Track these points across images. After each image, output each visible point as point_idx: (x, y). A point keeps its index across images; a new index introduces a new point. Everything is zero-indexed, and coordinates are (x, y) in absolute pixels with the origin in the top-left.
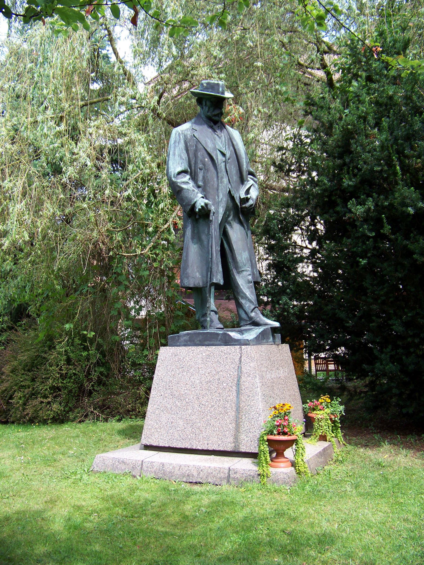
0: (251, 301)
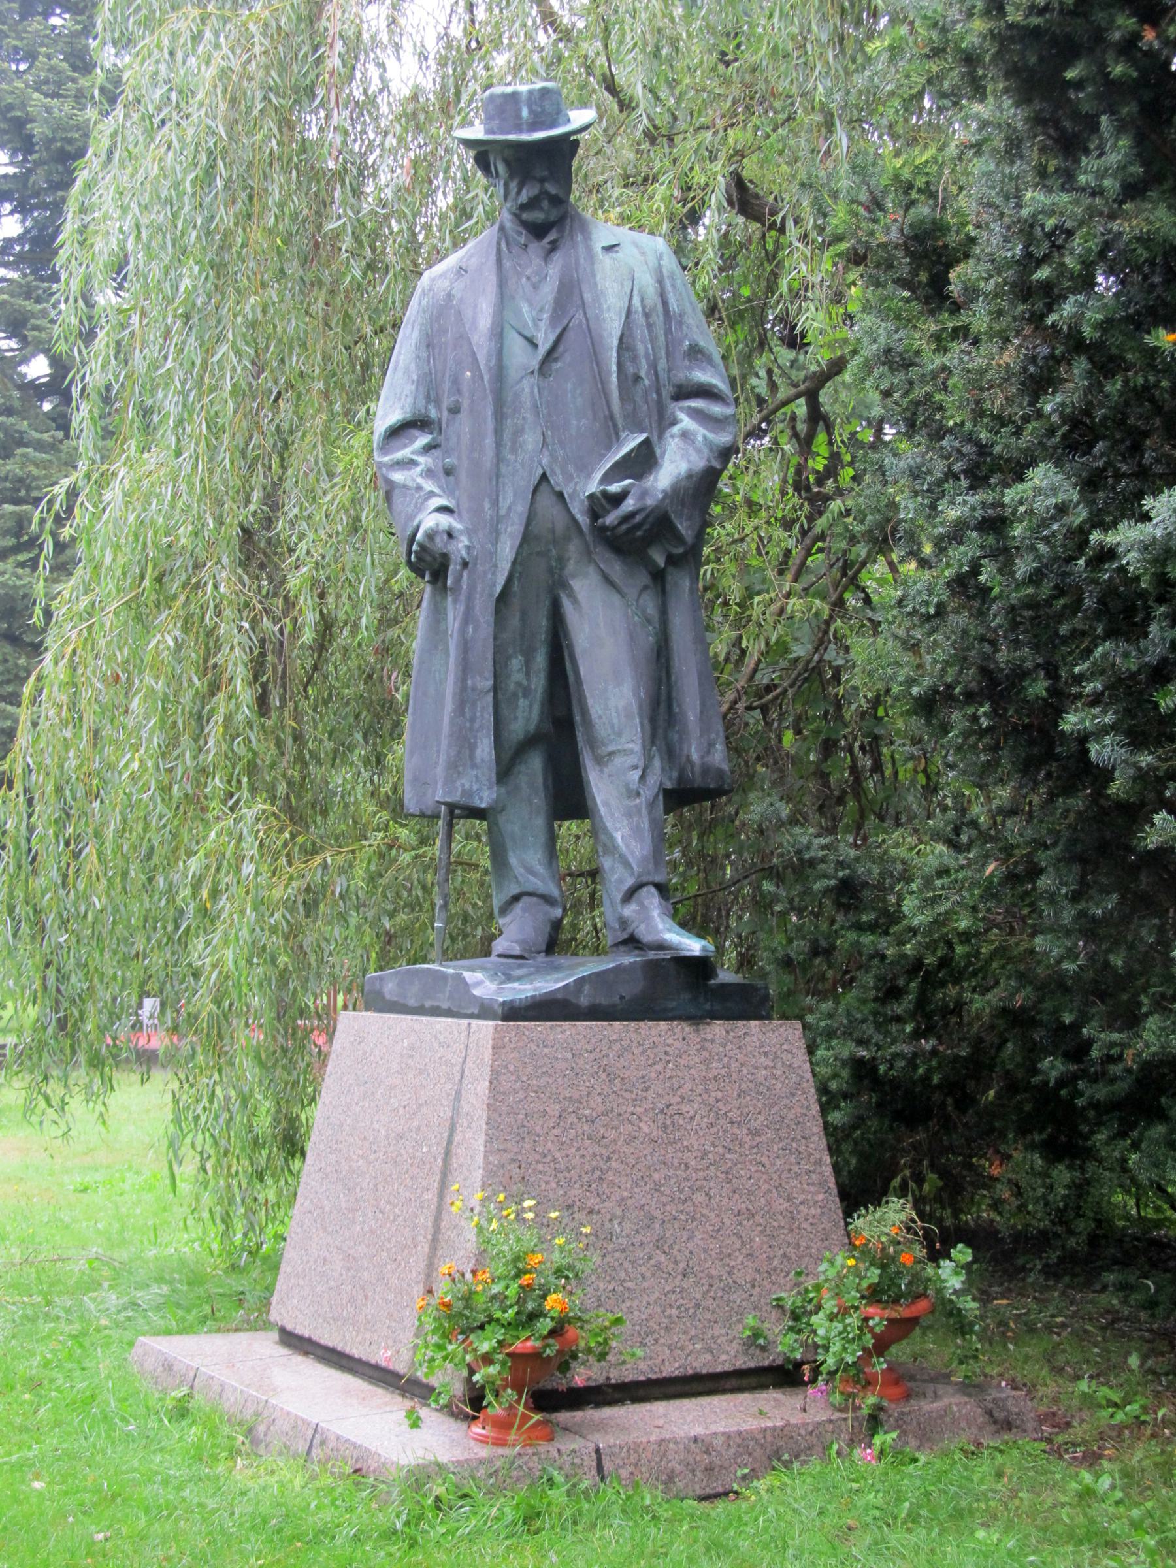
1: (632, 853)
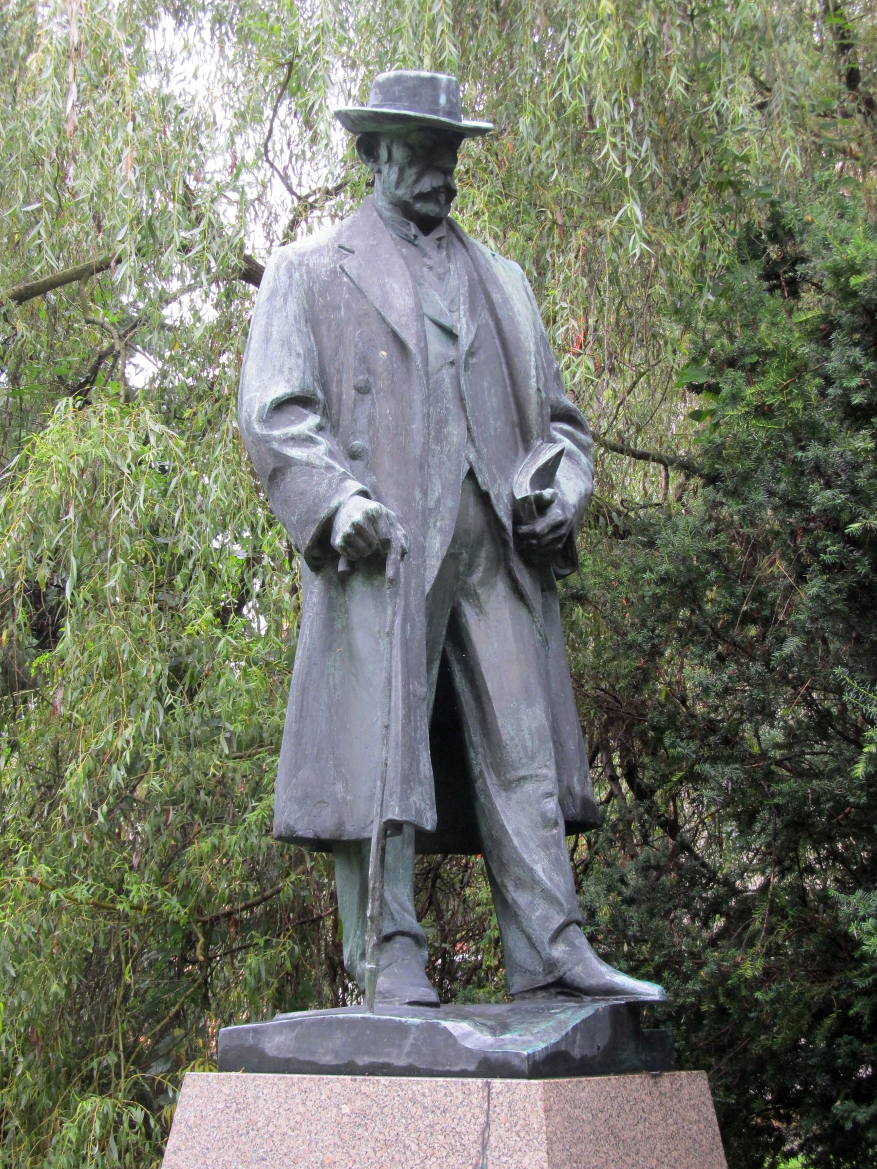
0: (551, 899)
1: (558, 887)
